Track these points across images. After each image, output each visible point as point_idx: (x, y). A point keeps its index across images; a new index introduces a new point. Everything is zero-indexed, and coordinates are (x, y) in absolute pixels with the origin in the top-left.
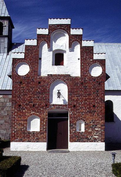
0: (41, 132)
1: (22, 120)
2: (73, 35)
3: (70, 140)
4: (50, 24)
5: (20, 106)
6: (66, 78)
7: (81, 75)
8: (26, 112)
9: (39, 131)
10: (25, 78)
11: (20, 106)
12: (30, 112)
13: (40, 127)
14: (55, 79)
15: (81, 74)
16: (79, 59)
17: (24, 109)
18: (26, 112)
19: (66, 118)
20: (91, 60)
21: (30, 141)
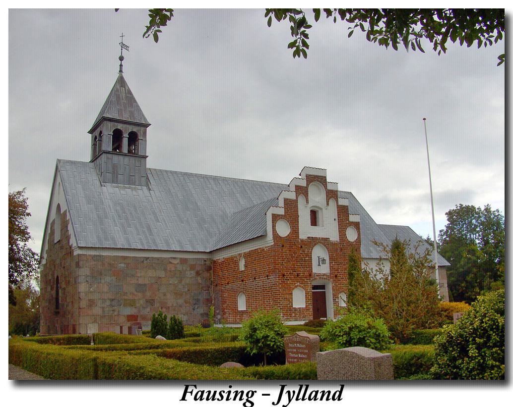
0: (307, 309)
1: (287, 294)
2: (329, 190)
3: (88, 344)
4: (341, 204)
5: (284, 275)
6: (325, 242)
7: (340, 240)
8: (291, 284)
9: (305, 307)
10: (286, 240)
11: (284, 275)
12: (295, 284)
13: (306, 302)
14: (313, 241)
15: (340, 238)
16: (335, 220)
17: (288, 280)
18: (291, 284)
19: (314, 289)
20: (347, 222)
21: (297, 320)
